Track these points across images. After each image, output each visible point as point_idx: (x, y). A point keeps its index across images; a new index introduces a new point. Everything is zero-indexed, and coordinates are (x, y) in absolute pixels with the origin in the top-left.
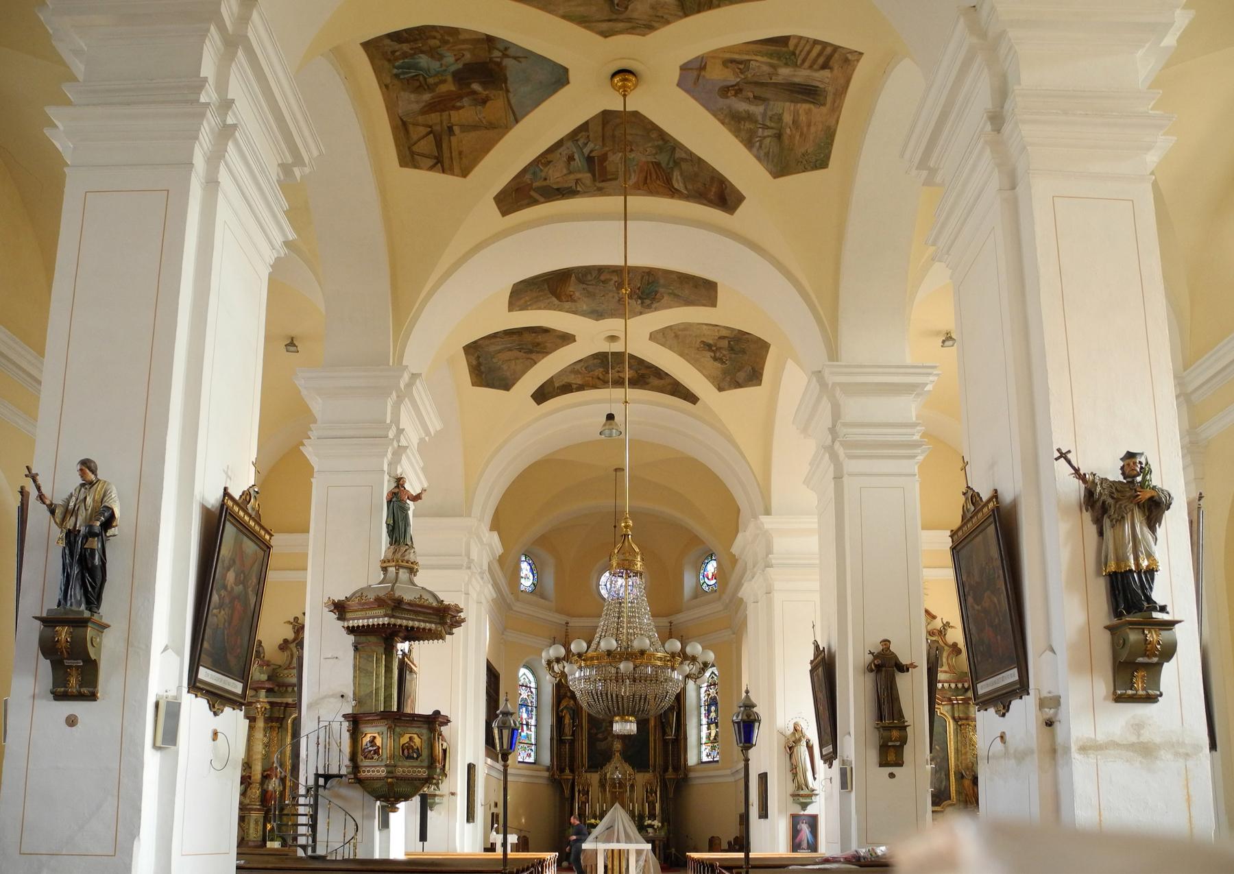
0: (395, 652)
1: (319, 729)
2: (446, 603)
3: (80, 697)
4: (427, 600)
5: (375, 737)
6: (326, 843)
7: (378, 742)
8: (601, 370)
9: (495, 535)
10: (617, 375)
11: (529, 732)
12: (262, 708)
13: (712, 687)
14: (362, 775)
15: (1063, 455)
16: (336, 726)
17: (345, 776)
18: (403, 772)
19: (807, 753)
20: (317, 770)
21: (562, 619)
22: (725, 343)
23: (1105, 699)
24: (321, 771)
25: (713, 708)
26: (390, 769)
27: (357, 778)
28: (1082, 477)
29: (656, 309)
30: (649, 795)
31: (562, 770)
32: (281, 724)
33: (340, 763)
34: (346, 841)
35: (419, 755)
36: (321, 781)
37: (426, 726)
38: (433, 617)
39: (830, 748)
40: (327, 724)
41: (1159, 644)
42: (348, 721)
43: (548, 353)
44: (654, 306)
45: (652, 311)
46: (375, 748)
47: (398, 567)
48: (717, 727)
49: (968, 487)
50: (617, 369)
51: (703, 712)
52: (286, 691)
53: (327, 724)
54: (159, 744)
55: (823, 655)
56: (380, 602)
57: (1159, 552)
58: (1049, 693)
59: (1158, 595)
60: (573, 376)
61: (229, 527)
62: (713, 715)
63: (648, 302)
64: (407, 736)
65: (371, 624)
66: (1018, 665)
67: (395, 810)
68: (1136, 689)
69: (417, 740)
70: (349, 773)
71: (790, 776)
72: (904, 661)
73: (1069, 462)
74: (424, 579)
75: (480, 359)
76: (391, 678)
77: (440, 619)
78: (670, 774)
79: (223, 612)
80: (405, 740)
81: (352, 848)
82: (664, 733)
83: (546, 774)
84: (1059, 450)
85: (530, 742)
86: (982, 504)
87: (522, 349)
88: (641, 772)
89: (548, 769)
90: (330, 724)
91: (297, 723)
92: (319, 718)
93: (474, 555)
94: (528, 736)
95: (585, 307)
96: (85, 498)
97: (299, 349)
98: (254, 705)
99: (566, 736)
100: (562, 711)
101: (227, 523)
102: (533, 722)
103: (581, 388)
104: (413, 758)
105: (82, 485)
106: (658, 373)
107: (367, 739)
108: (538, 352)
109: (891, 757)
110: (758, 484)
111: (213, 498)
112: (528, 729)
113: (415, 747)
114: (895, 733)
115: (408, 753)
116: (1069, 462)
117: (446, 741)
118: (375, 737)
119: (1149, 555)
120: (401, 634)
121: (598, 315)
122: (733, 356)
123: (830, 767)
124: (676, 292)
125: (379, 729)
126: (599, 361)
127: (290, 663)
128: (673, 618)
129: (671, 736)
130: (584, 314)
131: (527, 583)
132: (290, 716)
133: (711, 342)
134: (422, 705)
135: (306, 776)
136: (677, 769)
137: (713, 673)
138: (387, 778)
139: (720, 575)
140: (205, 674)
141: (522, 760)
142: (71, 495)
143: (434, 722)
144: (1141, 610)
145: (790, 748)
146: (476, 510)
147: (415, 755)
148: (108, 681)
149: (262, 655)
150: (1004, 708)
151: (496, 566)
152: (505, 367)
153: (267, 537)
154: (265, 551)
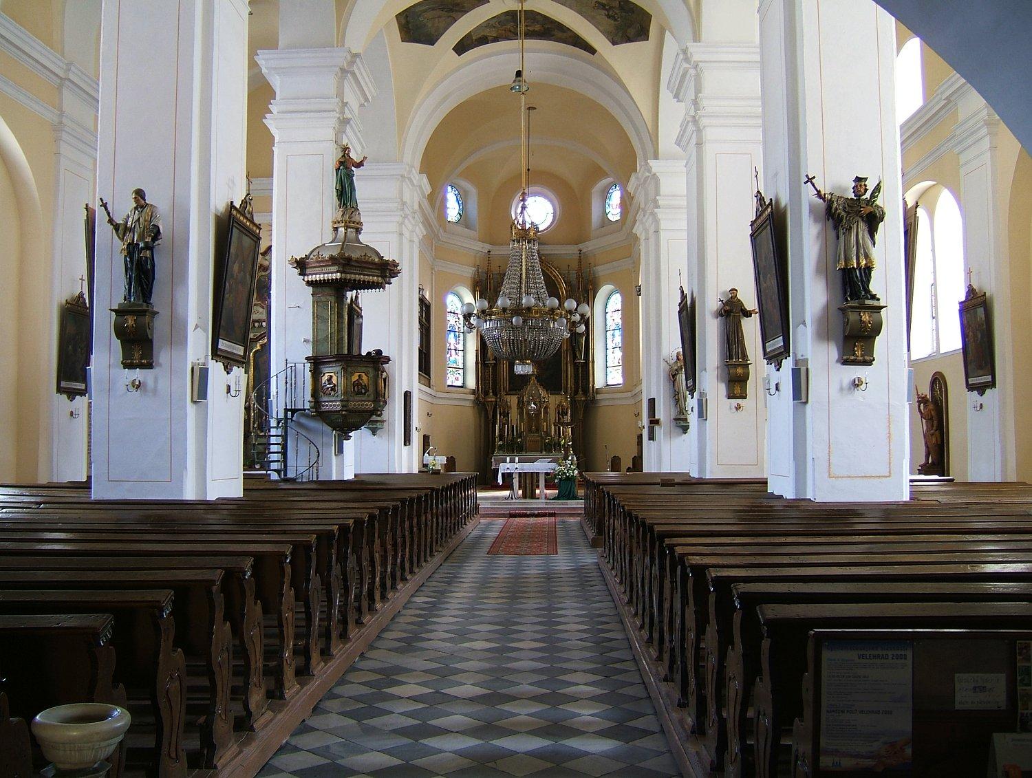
3: (142, 366)
5: (331, 376)
7: (334, 380)
9: (424, 180)
11: (456, 357)
14: (323, 409)
16: (300, 367)
21: (487, 247)
23: (837, 361)
26: (344, 403)
27: (319, 412)
31: (486, 393)
35: (367, 391)
36: (289, 413)
39: (779, 342)
41: (870, 323)
43: (466, 12)
47: (347, 227)
49: (758, 192)
53: (294, 365)
56: (333, 260)
57: (876, 253)
59: (873, 287)
61: (235, 230)
66: (783, 333)
67: (348, 438)
69: (365, 378)
70: (311, 408)
71: (673, 404)
73: (813, 185)
76: (343, 323)
80: (355, 378)
82: (575, 357)
83: (472, 397)
87: (444, 8)
89: (473, 392)
90: (295, 366)
93: (407, 198)
94: (455, 362)
96: (139, 218)
99: (490, 360)
101: (234, 228)
102: (460, 347)
103: (495, 40)
104: (362, 393)
105: (136, 208)
106: (560, 27)
107: (326, 378)
108: (456, 11)
109: (738, 391)
110: (649, 132)
113: (363, 384)
114: (740, 370)
116: (813, 185)
118: (331, 376)
119: (867, 256)
125: (335, 369)
126: (510, 17)
128: (581, 246)
131: (453, 212)
132: (252, 350)
138: (342, 411)
140: (223, 344)
141: (451, 384)
142: (128, 217)
143: (377, 360)
144: (858, 298)
145: (673, 376)
146: (408, 157)
147: (363, 391)
148: (163, 356)
151: (426, 204)
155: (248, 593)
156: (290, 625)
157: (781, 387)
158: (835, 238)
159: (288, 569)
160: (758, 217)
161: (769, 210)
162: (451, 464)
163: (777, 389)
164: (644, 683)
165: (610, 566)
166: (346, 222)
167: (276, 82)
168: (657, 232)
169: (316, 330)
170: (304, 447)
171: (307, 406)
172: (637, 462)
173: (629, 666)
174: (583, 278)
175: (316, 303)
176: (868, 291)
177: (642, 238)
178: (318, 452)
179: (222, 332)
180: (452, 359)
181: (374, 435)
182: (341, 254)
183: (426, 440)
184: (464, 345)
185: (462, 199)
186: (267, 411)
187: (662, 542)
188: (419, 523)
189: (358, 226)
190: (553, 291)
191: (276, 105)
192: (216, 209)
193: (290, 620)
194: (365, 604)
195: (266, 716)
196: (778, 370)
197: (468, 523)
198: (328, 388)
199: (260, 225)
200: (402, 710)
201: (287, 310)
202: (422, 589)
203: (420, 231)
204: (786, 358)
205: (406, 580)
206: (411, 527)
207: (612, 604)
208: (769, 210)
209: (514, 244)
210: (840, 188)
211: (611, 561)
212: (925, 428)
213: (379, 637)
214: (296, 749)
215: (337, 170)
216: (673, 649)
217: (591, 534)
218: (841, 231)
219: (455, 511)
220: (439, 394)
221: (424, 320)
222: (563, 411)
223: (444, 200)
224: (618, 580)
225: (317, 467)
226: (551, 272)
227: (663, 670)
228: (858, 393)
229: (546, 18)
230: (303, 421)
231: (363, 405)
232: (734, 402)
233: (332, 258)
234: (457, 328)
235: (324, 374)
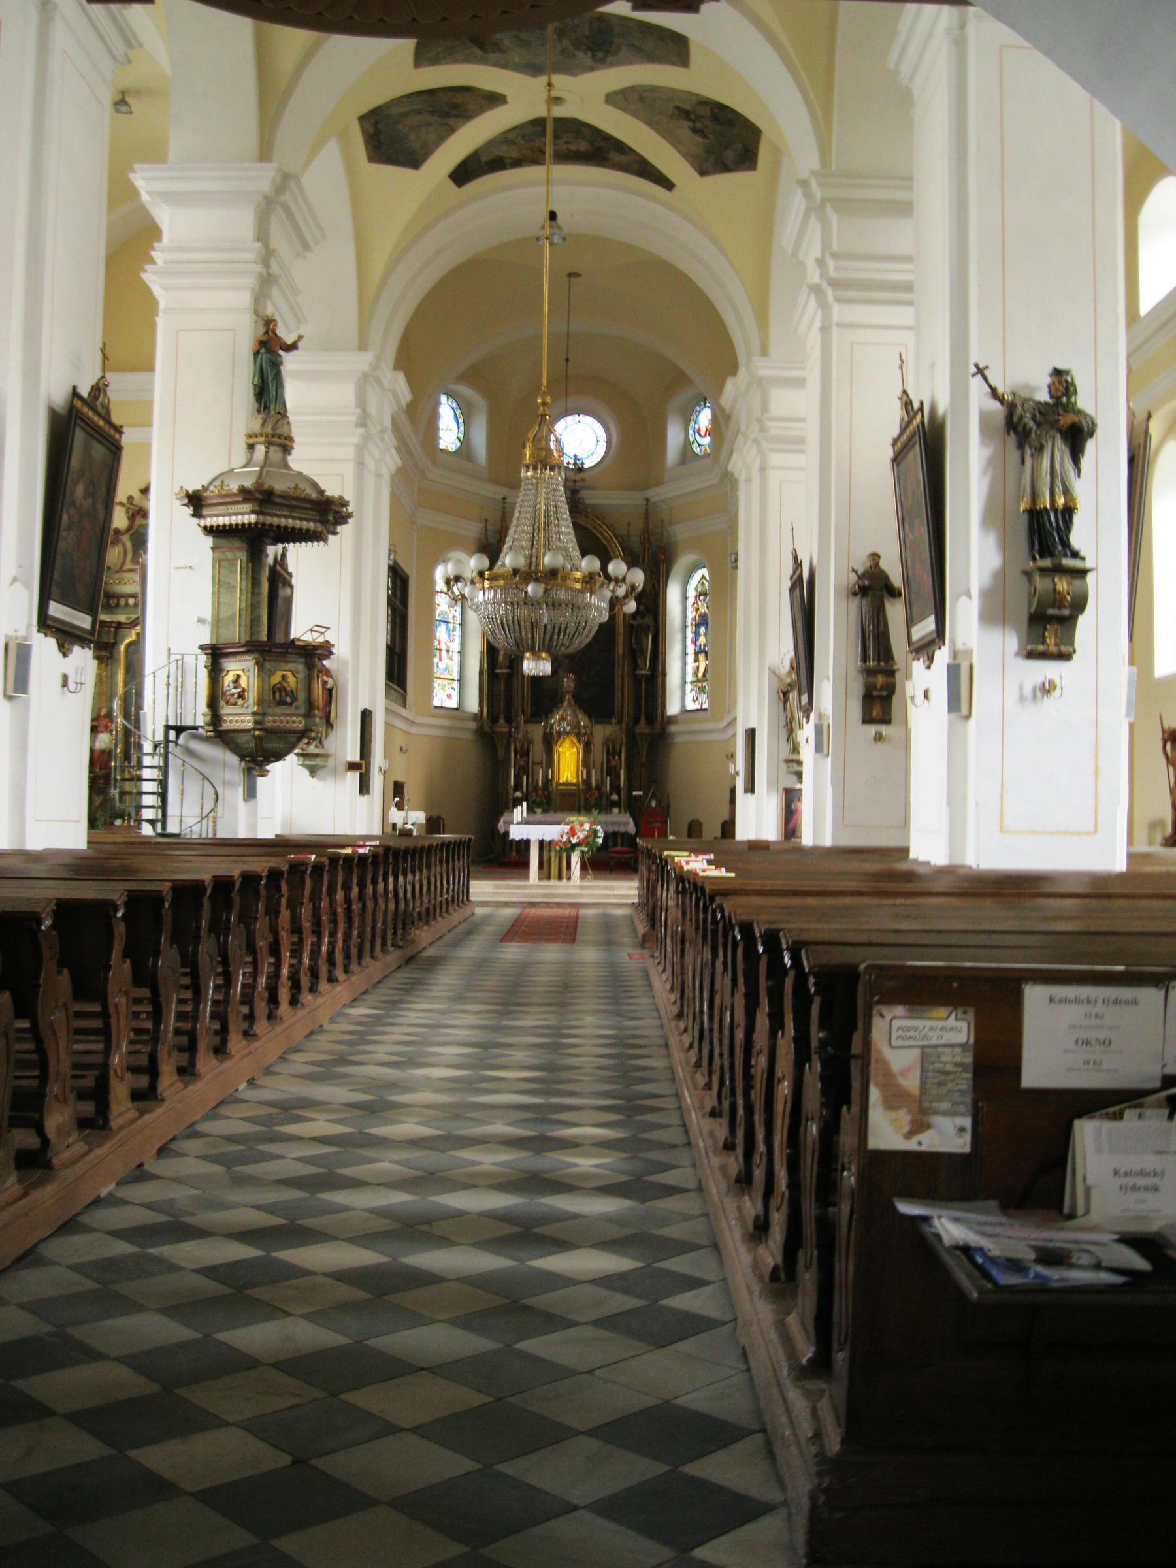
2: (329, 493)
4: (304, 490)
6: (179, 819)
7: (243, 682)
9: (401, 379)
10: (565, 147)
11: (450, 662)
13: (702, 598)
14: (226, 726)
15: (980, 371)
16: (190, 661)
17: (202, 727)
20: (167, 720)
23: (1017, 654)
24: (171, 723)
25: (703, 630)
26: (258, 718)
27: (221, 735)
29: (612, 65)
30: (611, 757)
32: (111, 653)
33: (197, 713)
34: (204, 815)
35: (294, 699)
37: (303, 660)
38: (311, 512)
40: (179, 657)
41: (1069, 594)
42: (206, 654)
44: (609, 60)
45: (606, 68)
46: (239, 690)
47: (269, 444)
50: (565, 139)
51: (690, 635)
52: (118, 605)
56: (246, 494)
57: (1083, 488)
59: (1077, 539)
60: (505, 148)
62: (702, 640)
63: (600, 55)
64: (279, 675)
68: (1048, 645)
71: (784, 735)
73: (985, 379)
74: (302, 460)
75: (379, 126)
76: (259, 594)
77: (321, 516)
78: (642, 728)
79: (72, 533)
80: (276, 679)
81: (211, 824)
82: (635, 666)
83: (473, 725)
84: (977, 366)
85: (450, 677)
88: (601, 723)
89: (476, 718)
91: (137, 647)
92: (169, 650)
94: (448, 669)
95: (517, 59)
97: (133, 109)
103: (517, 163)
106: (620, 147)
108: (457, 116)
111: (60, 398)
113: (289, 689)
114: (880, 680)
115: (280, 696)
116: (985, 379)
117: (332, 678)
118: (238, 677)
119: (1067, 492)
120: (272, 534)
121: (534, 69)
122: (718, 128)
124: (637, 43)
127: (123, 564)
129: (645, 671)
130: (517, 68)
132: (123, 641)
133: (688, 108)
134: (301, 629)
135: (153, 727)
136: (651, 720)
137: (703, 577)
138: (254, 729)
139: (717, 429)
140: (56, 610)
144: (1051, 555)
151: (404, 420)
152: (413, 137)
153: (117, 436)
155: (46, 953)
156: (122, 1017)
157: (932, 695)
158: (1020, 461)
159: (120, 929)
160: (903, 430)
161: (919, 418)
162: (433, 824)
163: (926, 696)
164: (684, 1125)
165: (660, 968)
166: (267, 436)
167: (163, 216)
168: (763, 469)
169: (217, 604)
170: (193, 788)
171: (200, 722)
172: (728, 828)
173: (670, 1103)
174: (650, 543)
175: (218, 563)
176: (1066, 544)
177: (742, 478)
178: (216, 793)
179: (55, 590)
180: (442, 665)
181: (313, 777)
182: (259, 484)
183: (399, 789)
184: (462, 644)
185: (466, 413)
186: (138, 727)
187: (712, 900)
188: (361, 897)
189: (287, 442)
190: (589, 543)
191: (162, 251)
192: (49, 398)
193: (123, 1009)
194: (261, 1008)
195: (73, 1149)
196: (929, 667)
199: (121, 427)
200: (300, 1154)
202: (365, 997)
203: (392, 461)
204: (940, 648)
205: (337, 981)
206: (348, 900)
207: (657, 1023)
208: (919, 418)
209: (527, 471)
210: (1027, 386)
211: (663, 962)
212: (1172, 781)
213: (283, 1059)
214: (124, 1202)
215: (256, 354)
216: (722, 1068)
217: (642, 929)
218: (1028, 452)
219: (429, 889)
220: (420, 720)
221: (398, 603)
222: (614, 749)
223: (434, 417)
224: (668, 986)
225: (215, 818)
226: (601, 534)
227: (711, 1101)
228: (1048, 703)
229: (596, 131)
230: (195, 745)
231: (287, 722)
232: (872, 729)
233: (243, 491)
234: (451, 616)
235: (228, 671)
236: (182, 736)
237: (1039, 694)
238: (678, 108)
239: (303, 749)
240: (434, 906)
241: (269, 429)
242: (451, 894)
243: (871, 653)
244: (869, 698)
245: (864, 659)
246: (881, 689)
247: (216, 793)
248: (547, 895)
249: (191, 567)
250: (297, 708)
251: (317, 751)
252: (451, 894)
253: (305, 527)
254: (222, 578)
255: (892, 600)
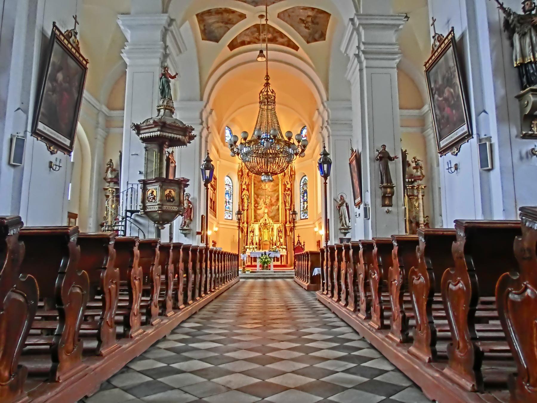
0: (164, 153)
1: (127, 189)
7: (155, 194)
8: (257, 34)
11: (229, 206)
12: (112, 191)
14: (148, 210)
18: (166, 208)
19: (346, 209)
20: (126, 208)
22: (309, 19)
24: (129, 209)
26: (160, 206)
27: (148, 214)
28: (504, 10)
30: (279, 233)
35: (174, 200)
47: (165, 109)
48: (307, 203)
54: (12, 163)
55: (355, 154)
56: (156, 124)
58: (485, 135)
62: (305, 198)
65: (151, 135)
67: (163, 228)
69: (173, 193)
71: (339, 221)
72: (392, 155)
74: (177, 116)
80: (167, 192)
86: (444, 39)
98: (108, 190)
100: (243, 196)
107: (150, 192)
112: (229, 204)
113: (172, 196)
114: (389, 190)
115: (169, 199)
118: (153, 191)
122: (313, 26)
123: (359, 209)
133: (304, 19)
137: (305, 179)
138: (158, 210)
140: (41, 126)
143: (182, 184)
147: (172, 200)
149: (112, 166)
150: (457, 150)
152: (216, 31)
153: (85, 62)
154: (83, 70)
181: (185, 237)
197: (232, 279)
198: (151, 198)
199: (87, 60)
201: (130, 155)
215: (161, 78)
230: (138, 219)
232: (386, 209)
234: (229, 192)
235: (149, 190)
236: (133, 215)
237: (529, 156)
238: (301, 19)
239: (182, 228)
240: (226, 276)
241: (165, 103)
242: (232, 273)
243: (384, 180)
244: (384, 197)
245: (382, 183)
246: (389, 194)
247: (144, 235)
248: (264, 275)
249: (137, 155)
250: (175, 203)
251: (187, 228)
252: (232, 273)
253: (178, 137)
254: (149, 158)
255: (391, 162)
